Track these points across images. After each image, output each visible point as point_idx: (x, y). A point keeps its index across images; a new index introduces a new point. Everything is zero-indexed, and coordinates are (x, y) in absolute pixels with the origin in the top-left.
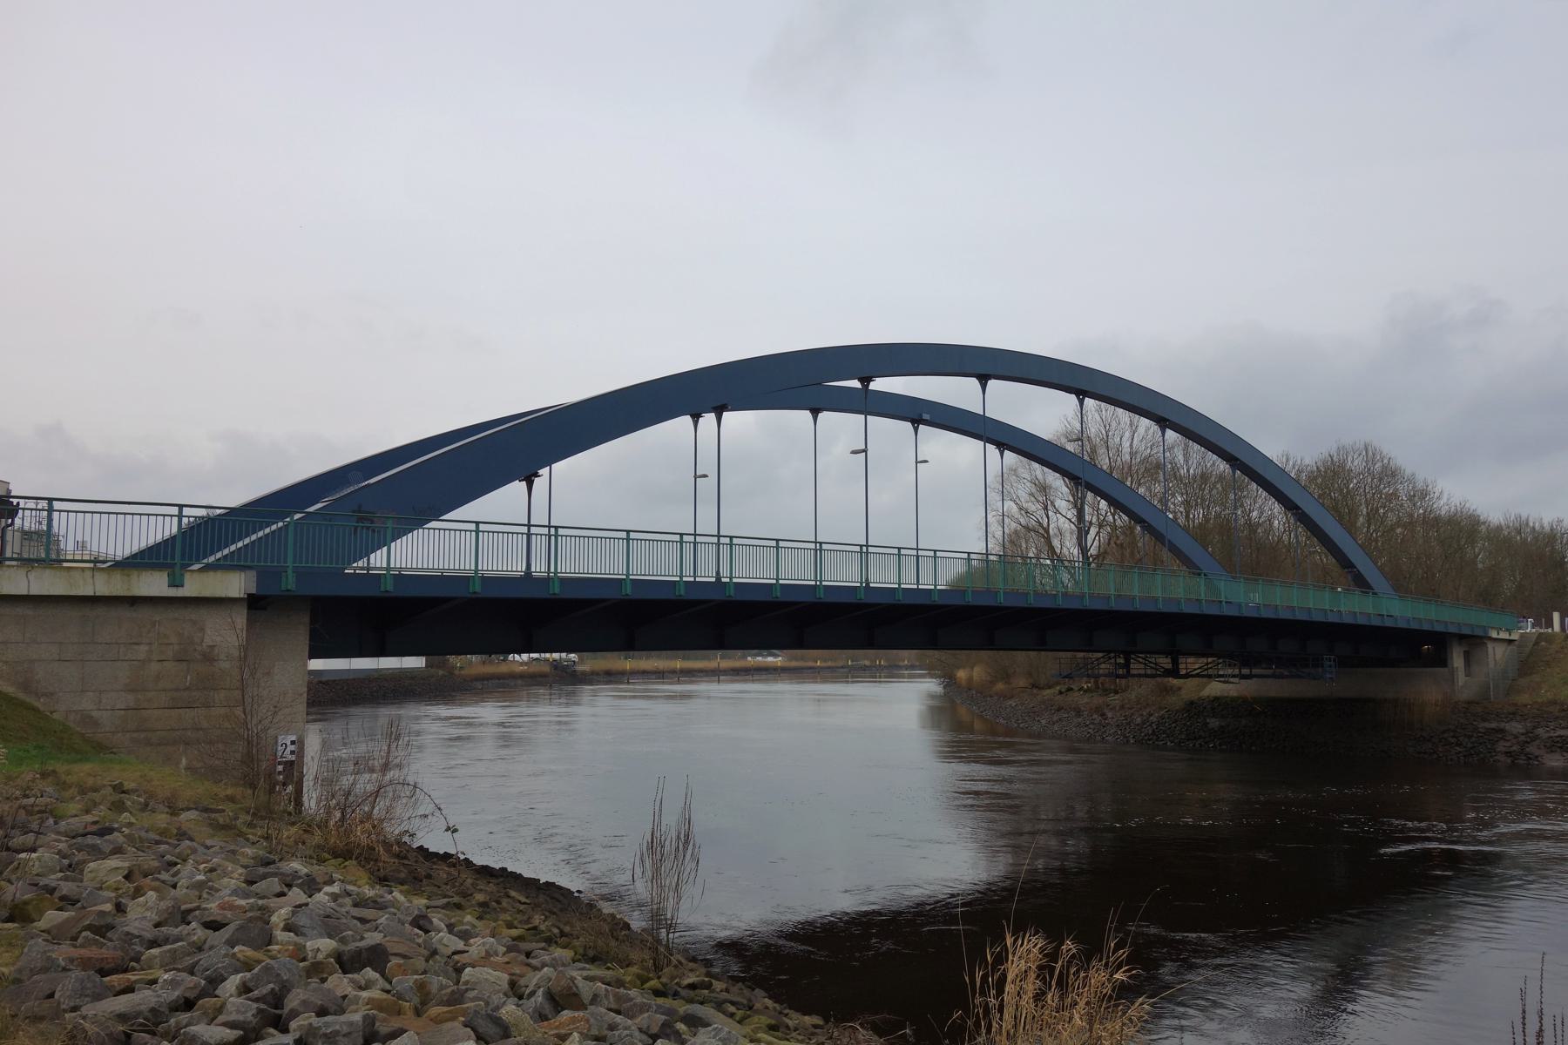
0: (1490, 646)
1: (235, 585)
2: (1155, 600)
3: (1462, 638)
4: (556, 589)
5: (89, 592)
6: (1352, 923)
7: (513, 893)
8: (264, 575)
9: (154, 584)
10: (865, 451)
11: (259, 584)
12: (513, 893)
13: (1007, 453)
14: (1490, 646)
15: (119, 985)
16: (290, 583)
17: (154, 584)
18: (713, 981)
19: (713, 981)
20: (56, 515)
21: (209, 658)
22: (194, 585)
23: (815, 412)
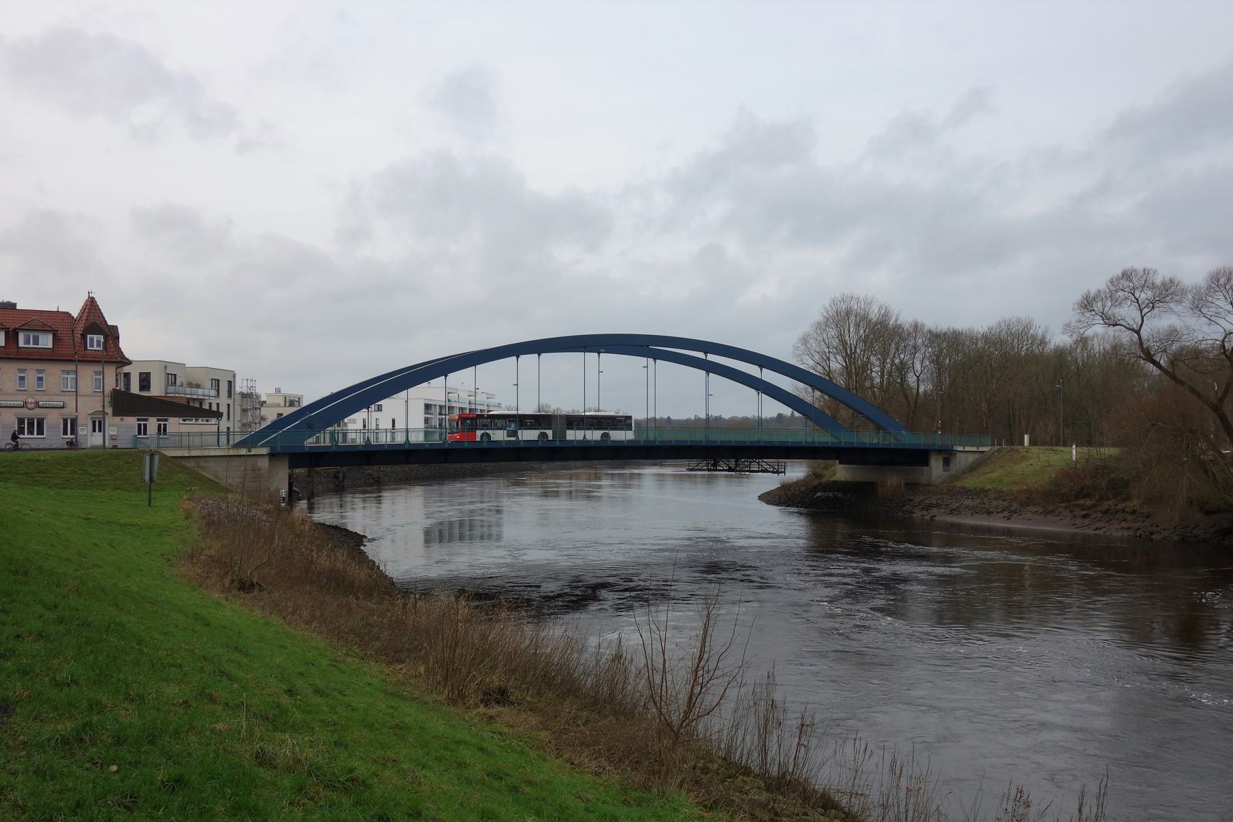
0: (958, 454)
1: (265, 451)
2: (853, 443)
3: (939, 451)
4: (762, 444)
5: (214, 455)
6: (1211, 661)
7: (346, 552)
8: (272, 448)
9: (243, 452)
10: (647, 367)
11: (271, 450)
12: (346, 552)
13: (764, 369)
14: (958, 454)
15: (331, 503)
16: (279, 450)
17: (243, 452)
18: (489, 432)
19: (489, 432)
20: (221, 436)
21: (259, 470)
22: (254, 451)
23: (599, 353)
